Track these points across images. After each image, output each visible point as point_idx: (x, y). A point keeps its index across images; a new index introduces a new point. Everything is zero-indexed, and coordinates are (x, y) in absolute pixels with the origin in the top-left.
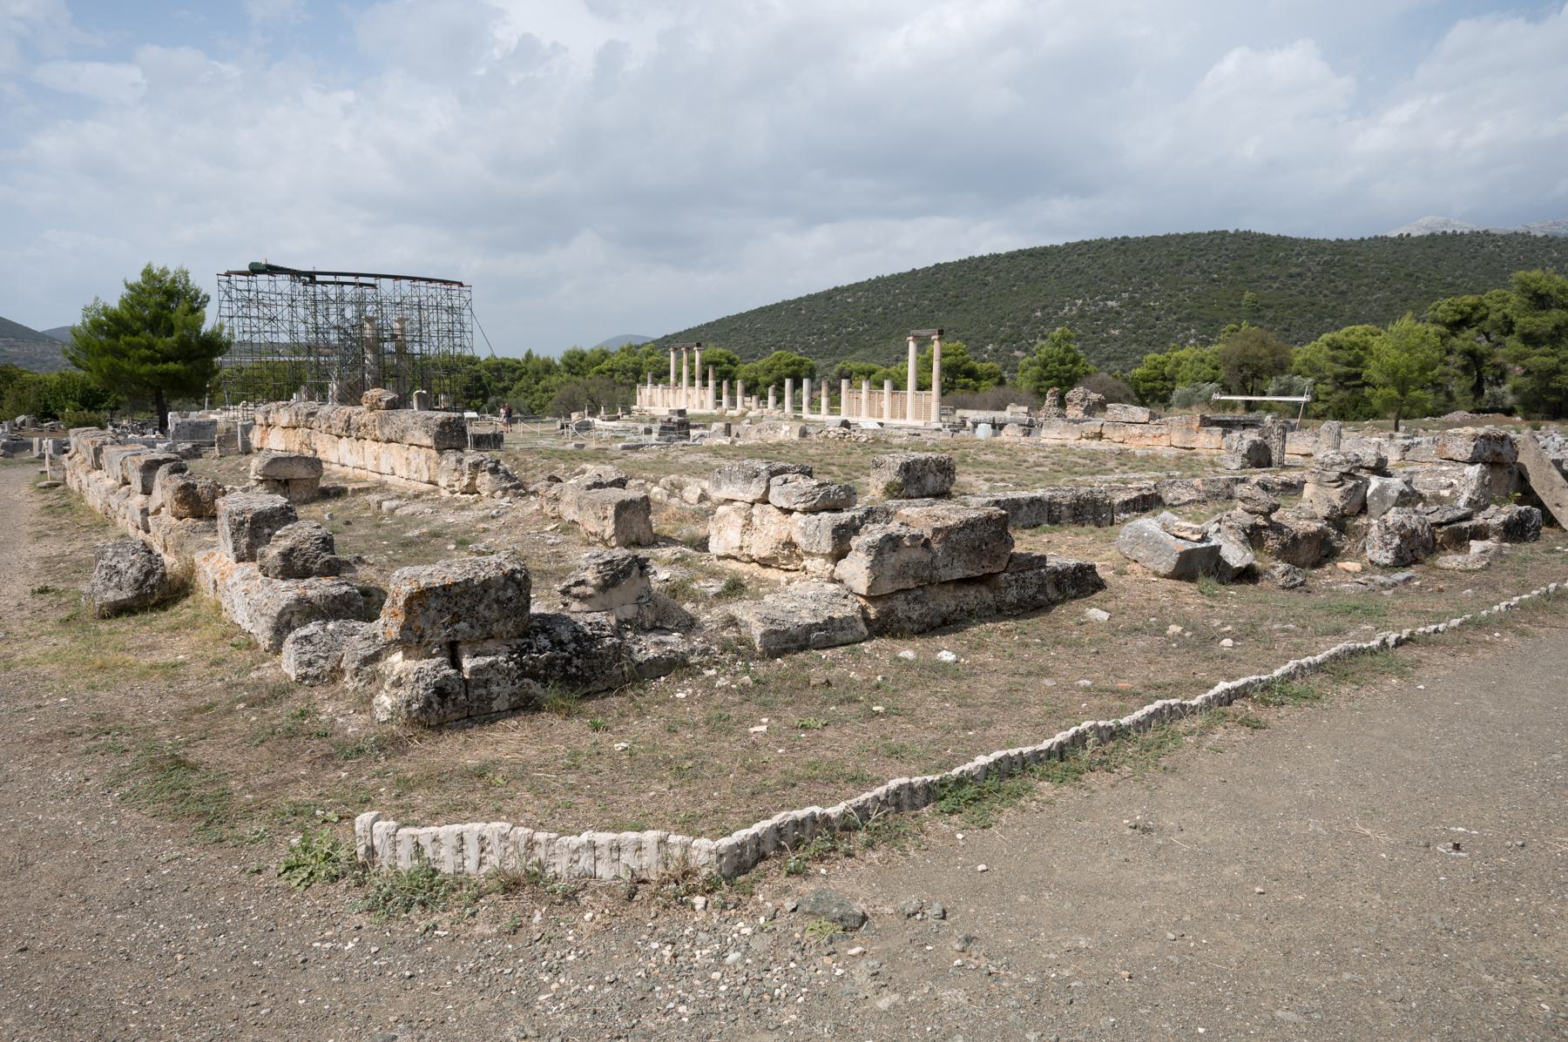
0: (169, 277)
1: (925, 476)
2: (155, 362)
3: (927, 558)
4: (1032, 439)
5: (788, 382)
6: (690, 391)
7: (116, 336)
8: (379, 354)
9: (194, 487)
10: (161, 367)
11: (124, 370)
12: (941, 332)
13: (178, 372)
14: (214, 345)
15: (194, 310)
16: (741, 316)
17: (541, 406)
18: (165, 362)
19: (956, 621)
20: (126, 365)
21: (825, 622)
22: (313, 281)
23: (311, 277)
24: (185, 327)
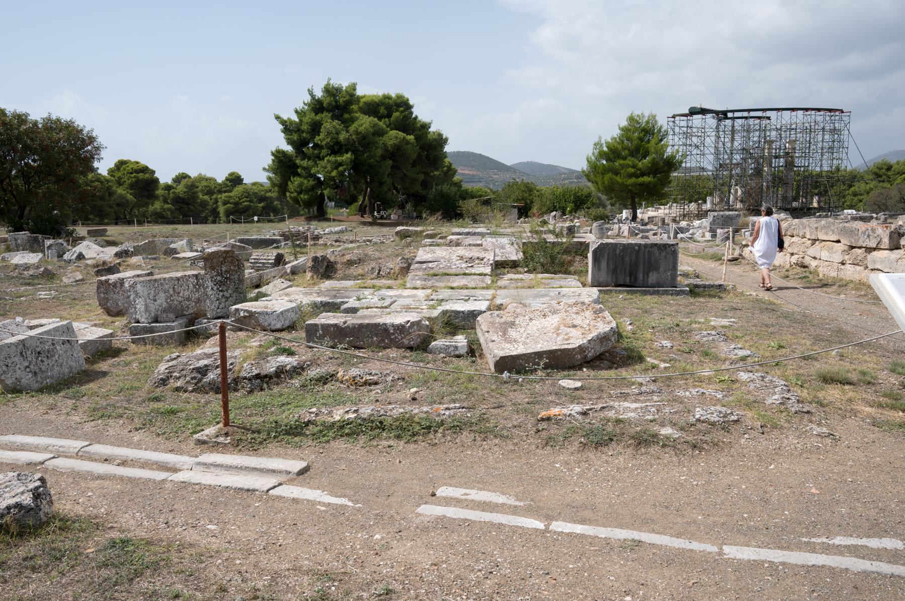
2: (637, 176)
10: (641, 180)
11: (618, 183)
13: (650, 183)
14: (671, 164)
20: (618, 178)
22: (726, 118)
23: (722, 115)
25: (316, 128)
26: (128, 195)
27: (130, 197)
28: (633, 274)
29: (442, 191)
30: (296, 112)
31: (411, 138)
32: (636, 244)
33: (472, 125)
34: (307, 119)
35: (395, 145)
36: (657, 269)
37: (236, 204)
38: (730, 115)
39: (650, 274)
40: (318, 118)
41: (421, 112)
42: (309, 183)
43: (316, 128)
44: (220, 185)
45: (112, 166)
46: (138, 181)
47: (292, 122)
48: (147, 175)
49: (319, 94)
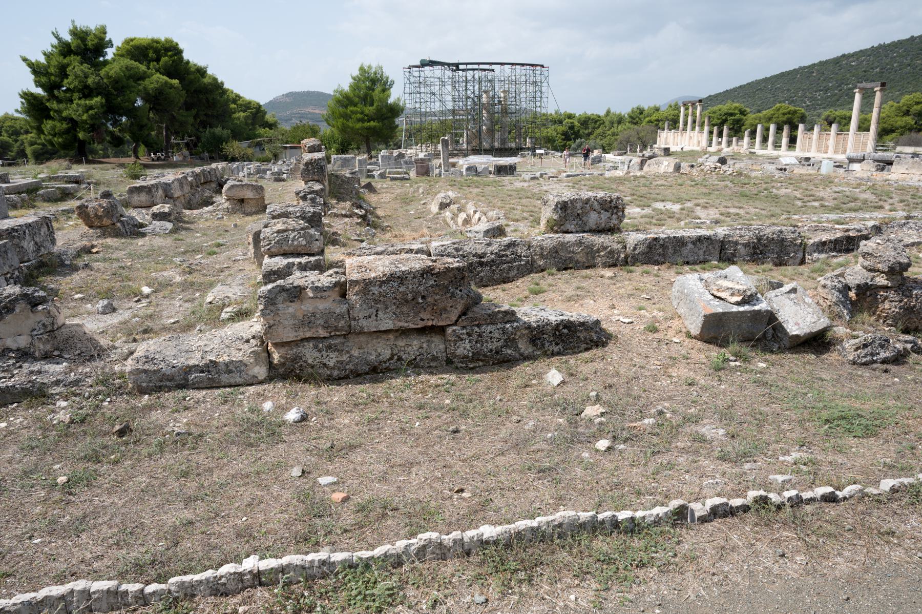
0: (373, 70)
1: (586, 214)
3: (341, 309)
4: (884, 175)
5: (772, 128)
6: (692, 134)
7: (346, 107)
8: (491, 114)
9: (87, 207)
10: (366, 124)
12: (883, 85)
14: (395, 111)
15: (384, 91)
16: (766, 80)
17: (610, 145)
18: (369, 121)
19: (388, 370)
21: (207, 365)
22: (458, 69)
23: (456, 67)
24: (380, 100)
25: (63, 72)
30: (45, 54)
31: (175, 82)
33: (249, 71)
34: (54, 62)
35: (157, 89)
38: (461, 67)
40: (65, 61)
41: (192, 55)
43: (63, 72)
47: (38, 63)
49: (68, 38)
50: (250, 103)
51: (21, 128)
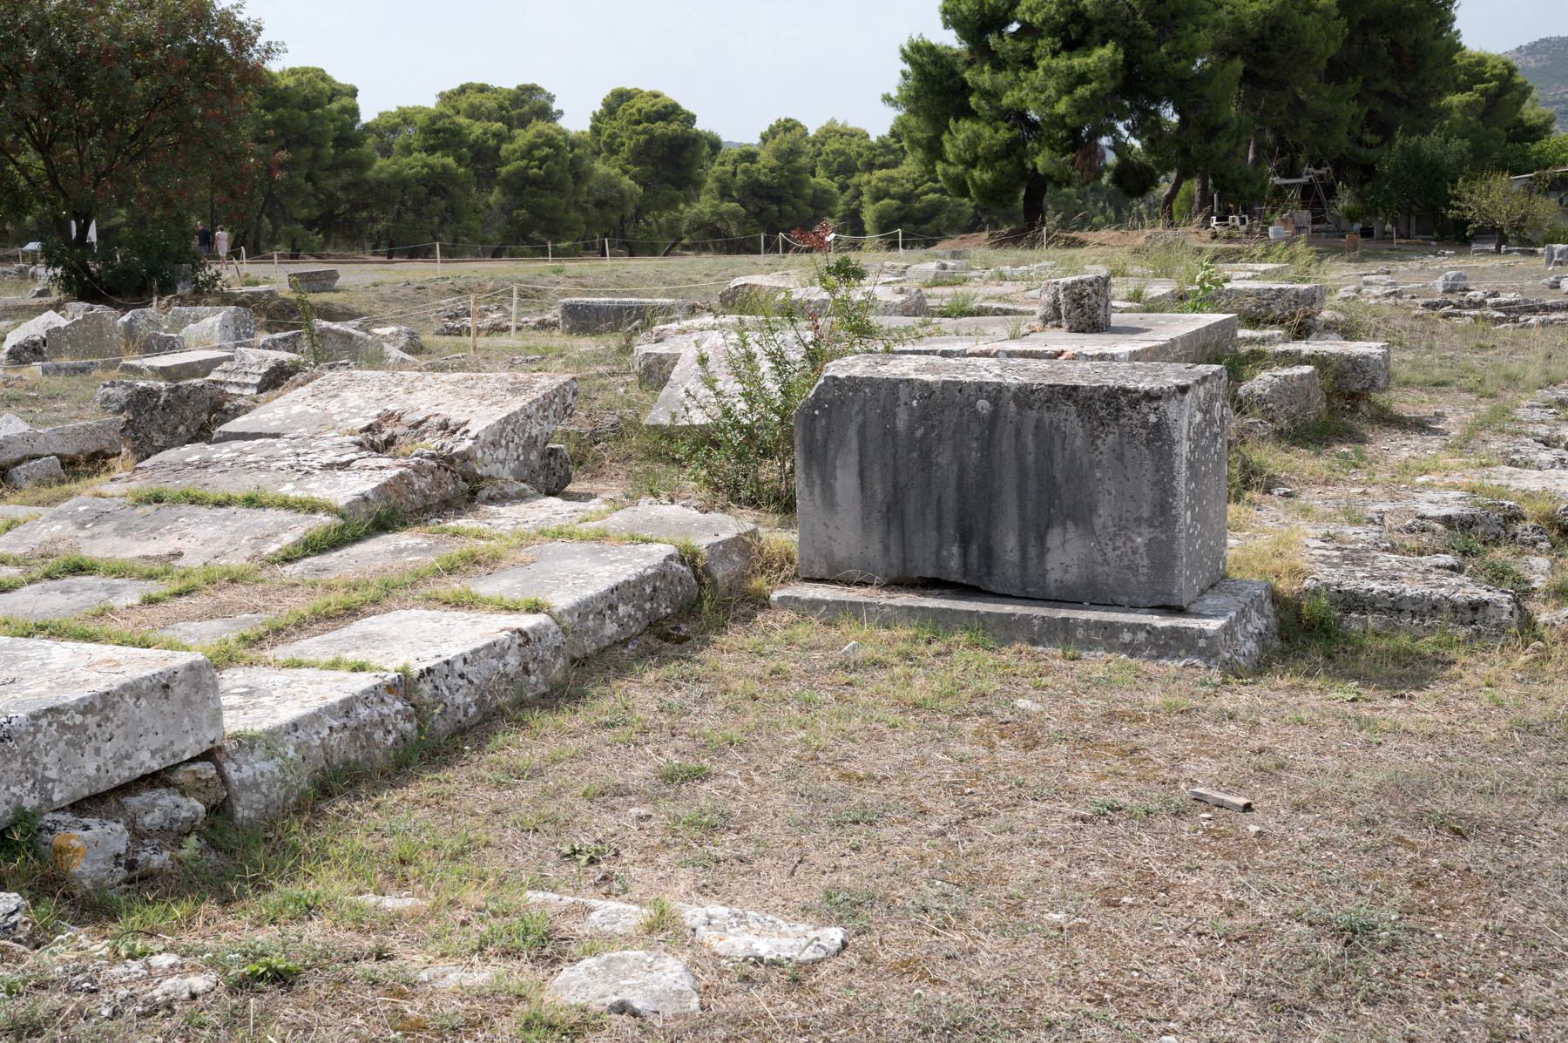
26: (626, 179)
27: (627, 182)
28: (972, 530)
29: (1417, 150)
32: (980, 387)
35: (1267, 16)
36: (1082, 515)
37: (906, 198)
39: (1054, 538)
42: (995, 136)
44: (871, 148)
45: (598, 107)
46: (652, 140)
48: (674, 126)
50: (1481, 61)
51: (860, 155)
